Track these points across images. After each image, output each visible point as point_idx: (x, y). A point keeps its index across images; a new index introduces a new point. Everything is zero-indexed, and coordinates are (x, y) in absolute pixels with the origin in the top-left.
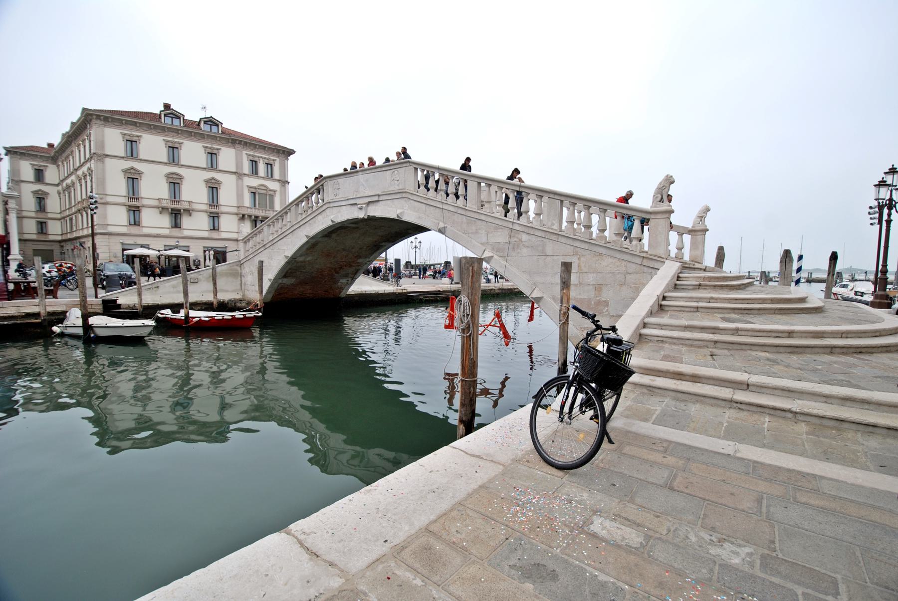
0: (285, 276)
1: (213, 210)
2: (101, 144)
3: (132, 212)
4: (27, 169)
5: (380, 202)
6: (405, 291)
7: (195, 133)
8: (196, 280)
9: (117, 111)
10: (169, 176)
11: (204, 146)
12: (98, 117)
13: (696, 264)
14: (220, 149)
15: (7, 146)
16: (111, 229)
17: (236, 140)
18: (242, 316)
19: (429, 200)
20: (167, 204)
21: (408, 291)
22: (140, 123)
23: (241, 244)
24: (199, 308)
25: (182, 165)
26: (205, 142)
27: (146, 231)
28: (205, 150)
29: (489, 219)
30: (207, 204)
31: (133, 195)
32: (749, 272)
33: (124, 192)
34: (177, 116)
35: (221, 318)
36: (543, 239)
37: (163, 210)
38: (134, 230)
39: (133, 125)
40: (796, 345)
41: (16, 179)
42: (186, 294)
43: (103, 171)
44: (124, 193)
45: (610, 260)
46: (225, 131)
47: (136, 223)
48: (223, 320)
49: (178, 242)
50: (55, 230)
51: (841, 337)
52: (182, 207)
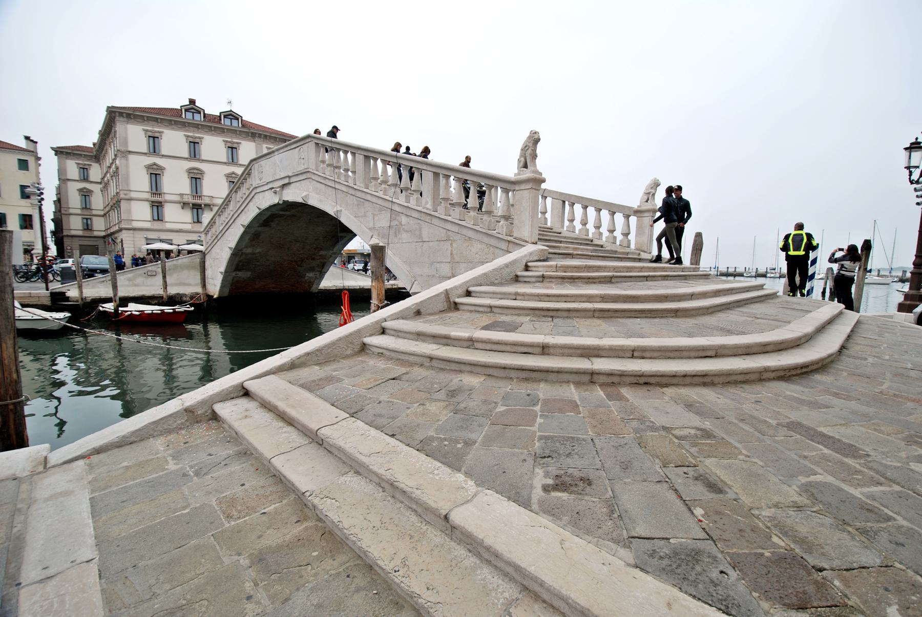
0: (237, 269)
1: (157, 199)
2: (125, 142)
3: (156, 207)
4: (73, 169)
5: (292, 185)
6: (396, 287)
7: (215, 127)
8: (154, 273)
9: (141, 108)
10: (190, 171)
11: (224, 141)
12: (121, 114)
13: (642, 253)
14: (202, 138)
15: (55, 146)
16: (136, 225)
17: (256, 133)
18: (171, 311)
19: (327, 180)
20: (191, 200)
21: (399, 286)
22: (161, 119)
23: (203, 235)
24: (156, 302)
25: (203, 160)
26: (226, 136)
27: (169, 226)
28: (225, 145)
29: (374, 200)
30: (148, 192)
31: (157, 190)
32: (728, 268)
33: (147, 187)
34: (198, 111)
35: (150, 312)
36: (419, 221)
37: (184, 205)
38: (158, 225)
39: (154, 121)
40: (531, 368)
41: (63, 178)
42: (115, 287)
43: (127, 166)
44: (147, 188)
45: (479, 246)
46: (245, 124)
47: (159, 218)
48: (152, 314)
49: (200, 237)
50: (99, 226)
51: (633, 357)
52: (203, 202)
